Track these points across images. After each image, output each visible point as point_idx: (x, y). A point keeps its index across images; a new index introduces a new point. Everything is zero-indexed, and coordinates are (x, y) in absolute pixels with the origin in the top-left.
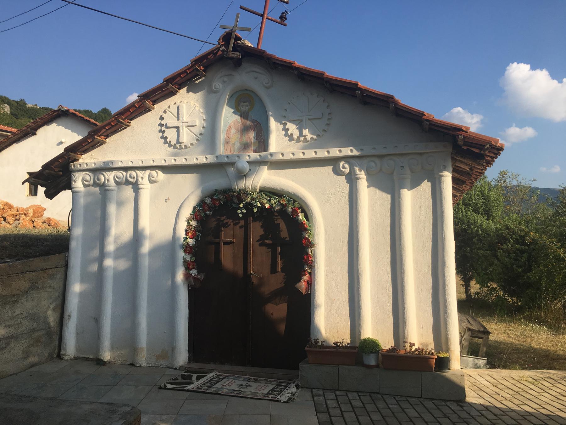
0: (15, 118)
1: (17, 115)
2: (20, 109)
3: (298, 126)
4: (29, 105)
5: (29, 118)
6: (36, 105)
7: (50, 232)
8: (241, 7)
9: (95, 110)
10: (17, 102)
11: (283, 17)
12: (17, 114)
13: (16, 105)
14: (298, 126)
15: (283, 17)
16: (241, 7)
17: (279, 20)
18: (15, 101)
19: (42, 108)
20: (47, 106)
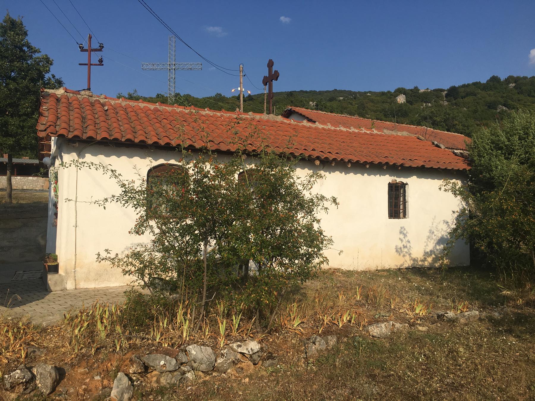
0: (410, 104)
1: (411, 102)
2: (414, 96)
3: (15, 172)
4: (422, 91)
5: (422, 102)
6: (428, 89)
7: (384, 332)
8: (80, 64)
9: (484, 81)
10: (411, 90)
11: (101, 61)
12: (411, 100)
13: (411, 92)
14: (15, 172)
15: (101, 61)
16: (80, 64)
17: (98, 63)
18: (410, 90)
19: (434, 90)
20: (437, 88)
